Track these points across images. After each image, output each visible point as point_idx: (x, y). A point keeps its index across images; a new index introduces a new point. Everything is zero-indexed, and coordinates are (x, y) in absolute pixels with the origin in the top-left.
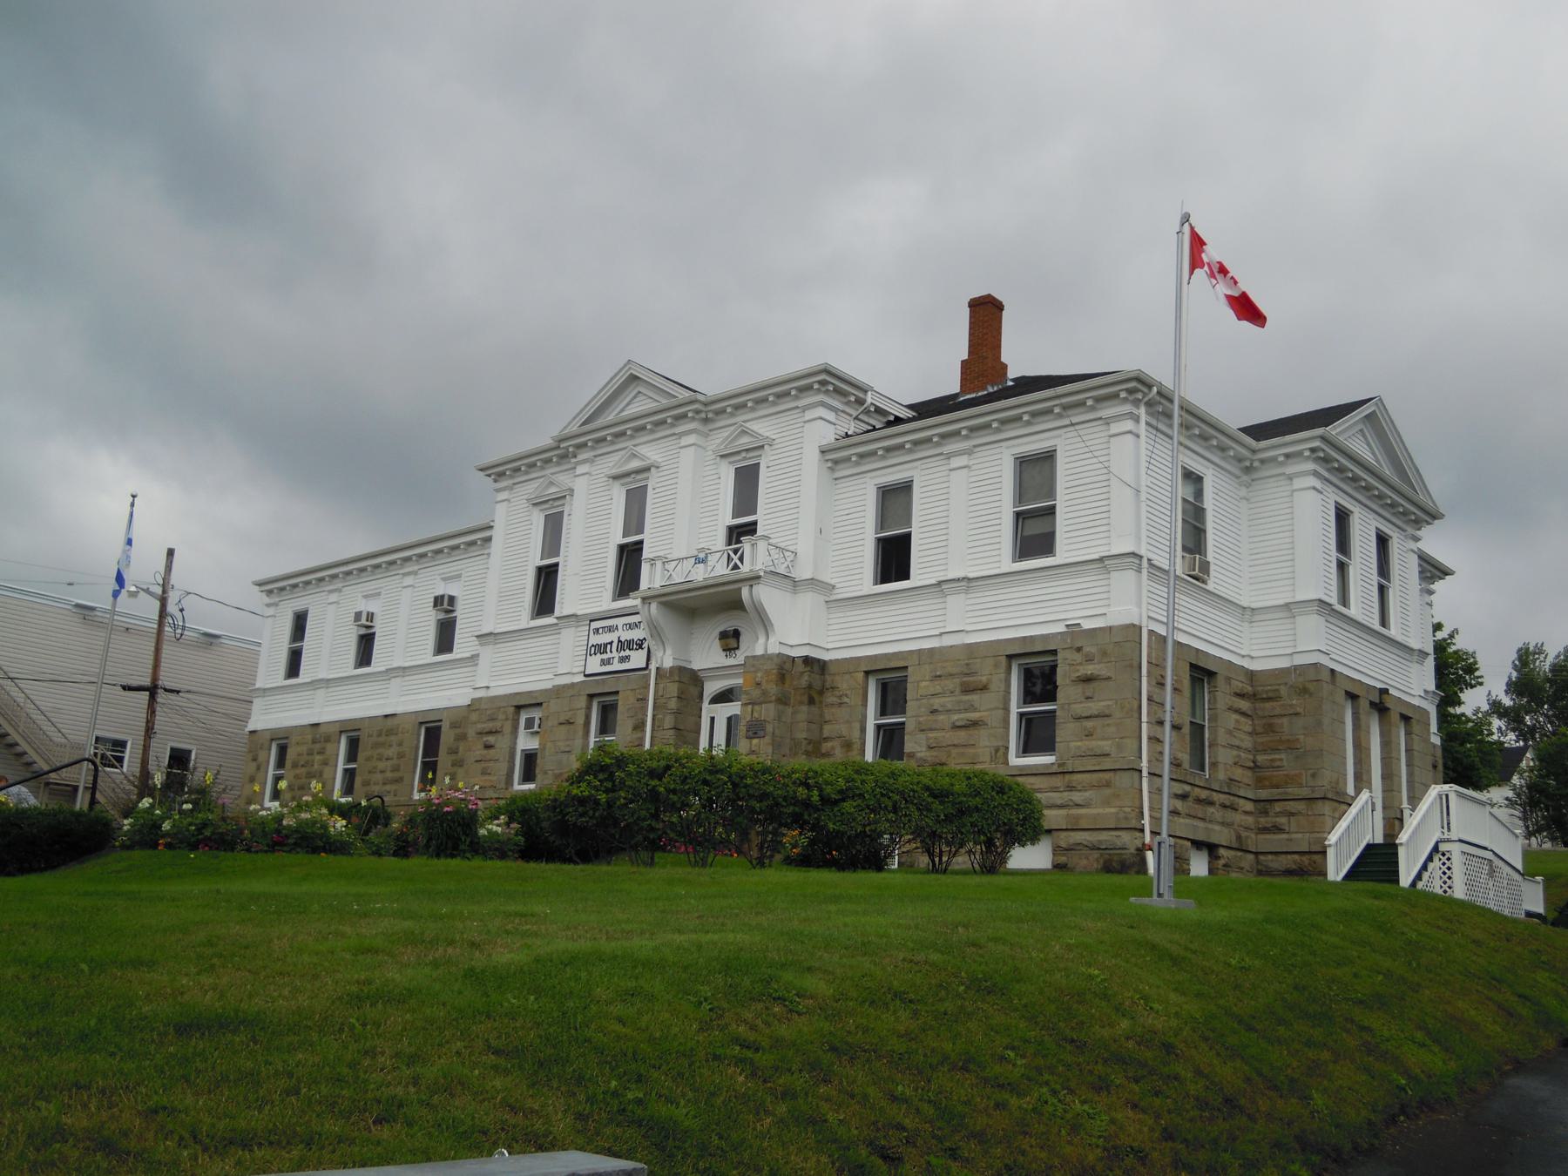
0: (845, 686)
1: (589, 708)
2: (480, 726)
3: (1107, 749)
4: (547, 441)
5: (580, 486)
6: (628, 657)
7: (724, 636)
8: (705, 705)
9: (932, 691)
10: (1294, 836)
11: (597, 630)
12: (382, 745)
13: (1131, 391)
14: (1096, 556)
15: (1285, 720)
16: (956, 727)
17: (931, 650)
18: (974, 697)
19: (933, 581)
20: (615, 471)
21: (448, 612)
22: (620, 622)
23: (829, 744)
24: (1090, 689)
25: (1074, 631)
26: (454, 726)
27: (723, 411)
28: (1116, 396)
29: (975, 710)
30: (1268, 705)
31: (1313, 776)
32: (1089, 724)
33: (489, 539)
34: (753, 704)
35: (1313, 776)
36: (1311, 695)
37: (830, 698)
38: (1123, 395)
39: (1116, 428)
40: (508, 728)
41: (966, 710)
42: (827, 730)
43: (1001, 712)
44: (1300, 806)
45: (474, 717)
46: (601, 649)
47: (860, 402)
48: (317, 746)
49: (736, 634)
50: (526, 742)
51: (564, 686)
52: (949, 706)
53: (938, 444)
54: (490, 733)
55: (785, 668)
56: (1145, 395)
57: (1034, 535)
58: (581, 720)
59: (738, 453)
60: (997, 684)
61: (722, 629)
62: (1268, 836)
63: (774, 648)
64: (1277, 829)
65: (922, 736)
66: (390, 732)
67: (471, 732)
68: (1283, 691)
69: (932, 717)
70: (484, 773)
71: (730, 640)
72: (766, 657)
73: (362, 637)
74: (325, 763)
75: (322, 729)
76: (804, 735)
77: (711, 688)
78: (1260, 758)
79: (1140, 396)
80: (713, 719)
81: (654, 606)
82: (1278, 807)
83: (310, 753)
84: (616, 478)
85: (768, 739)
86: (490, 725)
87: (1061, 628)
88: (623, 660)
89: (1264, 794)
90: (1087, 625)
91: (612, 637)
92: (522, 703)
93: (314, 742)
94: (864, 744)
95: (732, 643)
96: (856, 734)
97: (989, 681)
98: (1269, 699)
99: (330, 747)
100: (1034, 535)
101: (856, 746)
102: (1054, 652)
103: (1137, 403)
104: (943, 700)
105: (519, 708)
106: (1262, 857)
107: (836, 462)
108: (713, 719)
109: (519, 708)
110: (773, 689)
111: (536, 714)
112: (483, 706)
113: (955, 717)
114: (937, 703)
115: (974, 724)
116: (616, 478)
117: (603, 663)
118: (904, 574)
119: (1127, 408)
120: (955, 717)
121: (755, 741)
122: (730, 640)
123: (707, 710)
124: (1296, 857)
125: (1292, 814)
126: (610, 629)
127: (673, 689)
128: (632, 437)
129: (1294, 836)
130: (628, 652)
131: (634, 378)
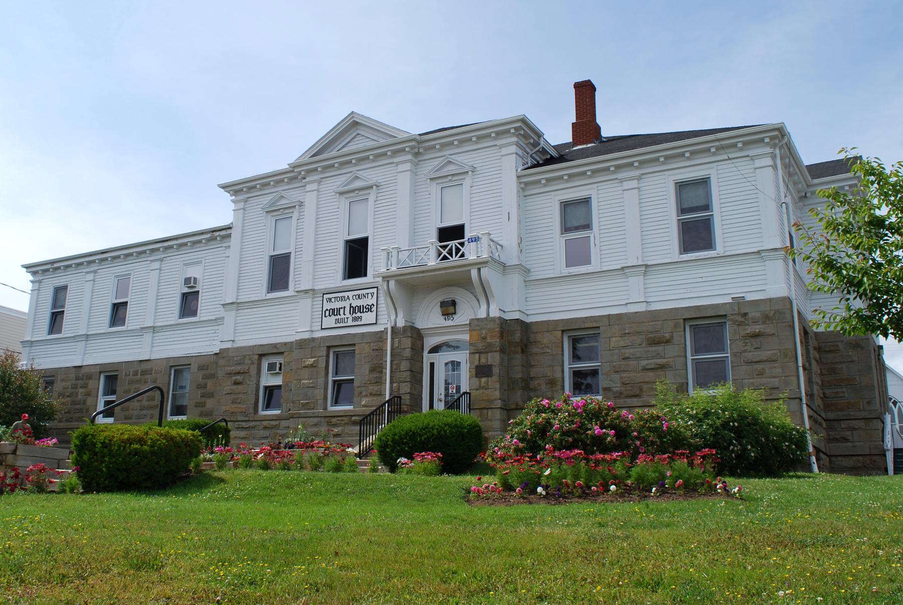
0: (545, 341)
1: (328, 356)
2: (229, 369)
3: (777, 385)
4: (284, 166)
5: (310, 200)
6: (360, 318)
7: (443, 304)
8: (425, 354)
9: (622, 344)
10: (857, 444)
11: (330, 299)
12: (139, 381)
13: (772, 138)
14: (755, 250)
15: (844, 366)
16: (645, 369)
17: (619, 316)
18: (660, 348)
19: (619, 267)
20: (341, 189)
21: (444, 247)
22: (350, 294)
23: (536, 382)
24: (756, 342)
25: (739, 302)
26: (201, 368)
27: (433, 147)
28: (762, 140)
29: (661, 357)
30: (830, 356)
31: (869, 403)
32: (759, 367)
33: (229, 236)
34: (480, 353)
35: (869, 403)
36: (862, 348)
37: (535, 350)
38: (767, 140)
39: (627, 185)
40: (253, 371)
41: (653, 358)
42: (533, 372)
43: (683, 358)
44: (861, 424)
45: (222, 362)
46: (334, 312)
47: (535, 144)
48: (80, 382)
49: (454, 303)
50: (269, 380)
51: (305, 340)
52: (638, 355)
53: (614, 172)
54: (238, 373)
55: (505, 326)
56: (780, 141)
57: (696, 234)
58: (322, 364)
59: (447, 176)
60: (677, 337)
61: (441, 299)
62: (836, 444)
63: (495, 313)
64: (845, 440)
65: (616, 377)
66: (144, 372)
67: (220, 374)
68: (841, 346)
69: (623, 363)
70: (234, 402)
71: (449, 308)
72: (488, 319)
73: (185, 296)
74: (88, 394)
75: (83, 371)
76: (520, 375)
77: (430, 342)
78: (828, 392)
79: (777, 141)
80: (432, 365)
81: (392, 283)
82: (844, 424)
83: (75, 387)
84: (341, 193)
85: (495, 378)
86: (238, 368)
87: (728, 300)
88: (355, 319)
89: (832, 415)
90: (750, 297)
91: (346, 304)
92: (566, 328)
93: (77, 379)
94: (563, 382)
95: (451, 309)
96: (559, 375)
97: (672, 337)
98: (830, 351)
99: (91, 383)
100: (696, 234)
101: (559, 383)
102: (354, 345)
103: (774, 146)
104: (631, 351)
105: (261, 356)
106: (833, 459)
107: (526, 184)
108: (432, 365)
109: (261, 356)
110: (496, 341)
111: (277, 360)
112: (231, 354)
113: (646, 362)
114: (628, 352)
115: (662, 367)
116: (341, 193)
117: (337, 321)
118: (194, 313)
119: (768, 150)
120: (646, 362)
121: (483, 380)
122: (449, 308)
123: (427, 358)
124: (860, 458)
125: (854, 429)
126: (342, 299)
127: (407, 342)
128: (356, 165)
129: (857, 444)
130: (359, 314)
131: (356, 124)
